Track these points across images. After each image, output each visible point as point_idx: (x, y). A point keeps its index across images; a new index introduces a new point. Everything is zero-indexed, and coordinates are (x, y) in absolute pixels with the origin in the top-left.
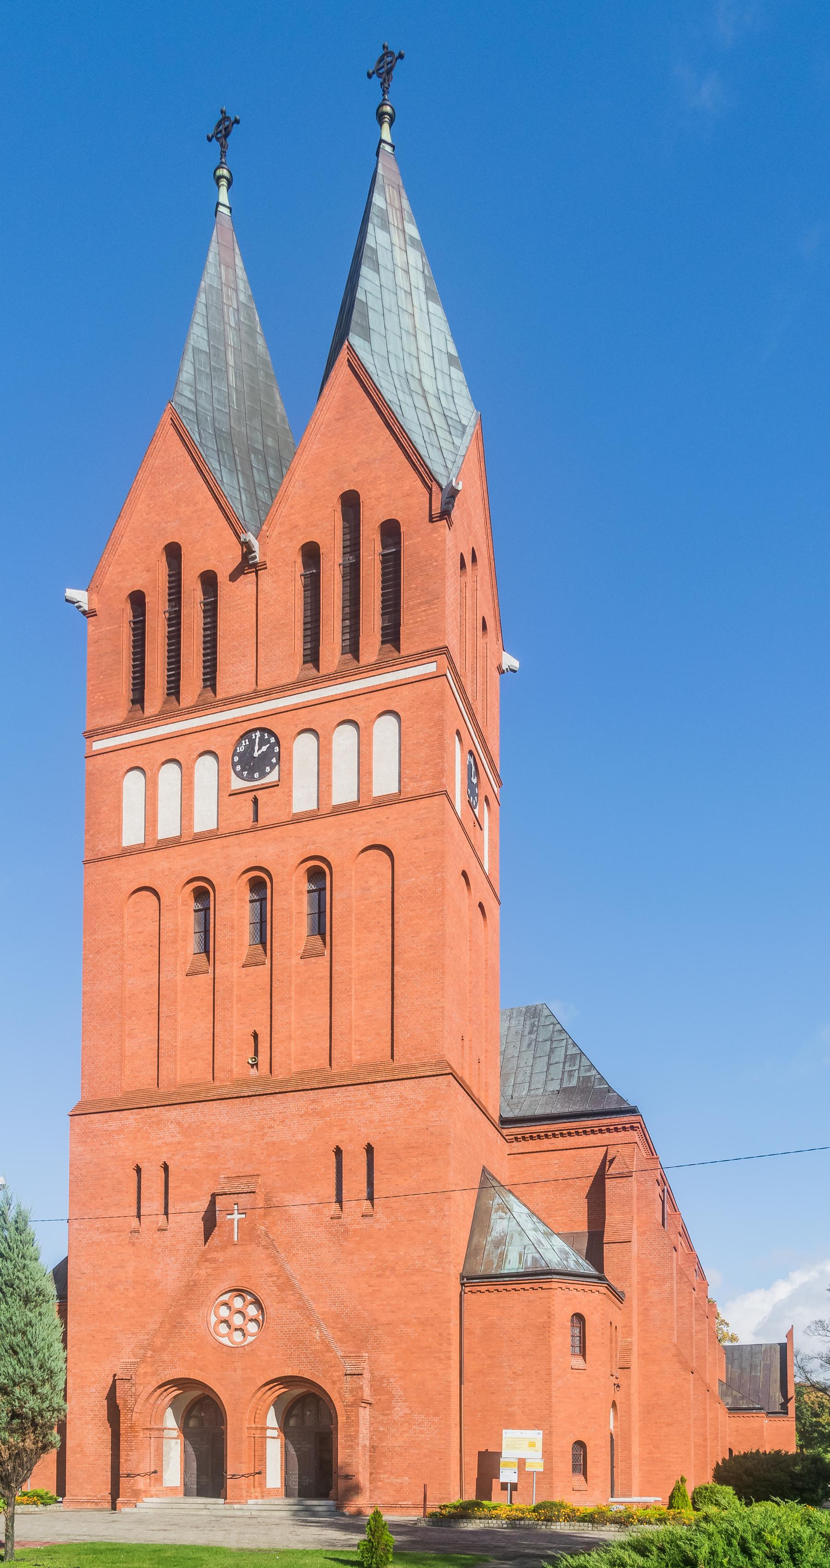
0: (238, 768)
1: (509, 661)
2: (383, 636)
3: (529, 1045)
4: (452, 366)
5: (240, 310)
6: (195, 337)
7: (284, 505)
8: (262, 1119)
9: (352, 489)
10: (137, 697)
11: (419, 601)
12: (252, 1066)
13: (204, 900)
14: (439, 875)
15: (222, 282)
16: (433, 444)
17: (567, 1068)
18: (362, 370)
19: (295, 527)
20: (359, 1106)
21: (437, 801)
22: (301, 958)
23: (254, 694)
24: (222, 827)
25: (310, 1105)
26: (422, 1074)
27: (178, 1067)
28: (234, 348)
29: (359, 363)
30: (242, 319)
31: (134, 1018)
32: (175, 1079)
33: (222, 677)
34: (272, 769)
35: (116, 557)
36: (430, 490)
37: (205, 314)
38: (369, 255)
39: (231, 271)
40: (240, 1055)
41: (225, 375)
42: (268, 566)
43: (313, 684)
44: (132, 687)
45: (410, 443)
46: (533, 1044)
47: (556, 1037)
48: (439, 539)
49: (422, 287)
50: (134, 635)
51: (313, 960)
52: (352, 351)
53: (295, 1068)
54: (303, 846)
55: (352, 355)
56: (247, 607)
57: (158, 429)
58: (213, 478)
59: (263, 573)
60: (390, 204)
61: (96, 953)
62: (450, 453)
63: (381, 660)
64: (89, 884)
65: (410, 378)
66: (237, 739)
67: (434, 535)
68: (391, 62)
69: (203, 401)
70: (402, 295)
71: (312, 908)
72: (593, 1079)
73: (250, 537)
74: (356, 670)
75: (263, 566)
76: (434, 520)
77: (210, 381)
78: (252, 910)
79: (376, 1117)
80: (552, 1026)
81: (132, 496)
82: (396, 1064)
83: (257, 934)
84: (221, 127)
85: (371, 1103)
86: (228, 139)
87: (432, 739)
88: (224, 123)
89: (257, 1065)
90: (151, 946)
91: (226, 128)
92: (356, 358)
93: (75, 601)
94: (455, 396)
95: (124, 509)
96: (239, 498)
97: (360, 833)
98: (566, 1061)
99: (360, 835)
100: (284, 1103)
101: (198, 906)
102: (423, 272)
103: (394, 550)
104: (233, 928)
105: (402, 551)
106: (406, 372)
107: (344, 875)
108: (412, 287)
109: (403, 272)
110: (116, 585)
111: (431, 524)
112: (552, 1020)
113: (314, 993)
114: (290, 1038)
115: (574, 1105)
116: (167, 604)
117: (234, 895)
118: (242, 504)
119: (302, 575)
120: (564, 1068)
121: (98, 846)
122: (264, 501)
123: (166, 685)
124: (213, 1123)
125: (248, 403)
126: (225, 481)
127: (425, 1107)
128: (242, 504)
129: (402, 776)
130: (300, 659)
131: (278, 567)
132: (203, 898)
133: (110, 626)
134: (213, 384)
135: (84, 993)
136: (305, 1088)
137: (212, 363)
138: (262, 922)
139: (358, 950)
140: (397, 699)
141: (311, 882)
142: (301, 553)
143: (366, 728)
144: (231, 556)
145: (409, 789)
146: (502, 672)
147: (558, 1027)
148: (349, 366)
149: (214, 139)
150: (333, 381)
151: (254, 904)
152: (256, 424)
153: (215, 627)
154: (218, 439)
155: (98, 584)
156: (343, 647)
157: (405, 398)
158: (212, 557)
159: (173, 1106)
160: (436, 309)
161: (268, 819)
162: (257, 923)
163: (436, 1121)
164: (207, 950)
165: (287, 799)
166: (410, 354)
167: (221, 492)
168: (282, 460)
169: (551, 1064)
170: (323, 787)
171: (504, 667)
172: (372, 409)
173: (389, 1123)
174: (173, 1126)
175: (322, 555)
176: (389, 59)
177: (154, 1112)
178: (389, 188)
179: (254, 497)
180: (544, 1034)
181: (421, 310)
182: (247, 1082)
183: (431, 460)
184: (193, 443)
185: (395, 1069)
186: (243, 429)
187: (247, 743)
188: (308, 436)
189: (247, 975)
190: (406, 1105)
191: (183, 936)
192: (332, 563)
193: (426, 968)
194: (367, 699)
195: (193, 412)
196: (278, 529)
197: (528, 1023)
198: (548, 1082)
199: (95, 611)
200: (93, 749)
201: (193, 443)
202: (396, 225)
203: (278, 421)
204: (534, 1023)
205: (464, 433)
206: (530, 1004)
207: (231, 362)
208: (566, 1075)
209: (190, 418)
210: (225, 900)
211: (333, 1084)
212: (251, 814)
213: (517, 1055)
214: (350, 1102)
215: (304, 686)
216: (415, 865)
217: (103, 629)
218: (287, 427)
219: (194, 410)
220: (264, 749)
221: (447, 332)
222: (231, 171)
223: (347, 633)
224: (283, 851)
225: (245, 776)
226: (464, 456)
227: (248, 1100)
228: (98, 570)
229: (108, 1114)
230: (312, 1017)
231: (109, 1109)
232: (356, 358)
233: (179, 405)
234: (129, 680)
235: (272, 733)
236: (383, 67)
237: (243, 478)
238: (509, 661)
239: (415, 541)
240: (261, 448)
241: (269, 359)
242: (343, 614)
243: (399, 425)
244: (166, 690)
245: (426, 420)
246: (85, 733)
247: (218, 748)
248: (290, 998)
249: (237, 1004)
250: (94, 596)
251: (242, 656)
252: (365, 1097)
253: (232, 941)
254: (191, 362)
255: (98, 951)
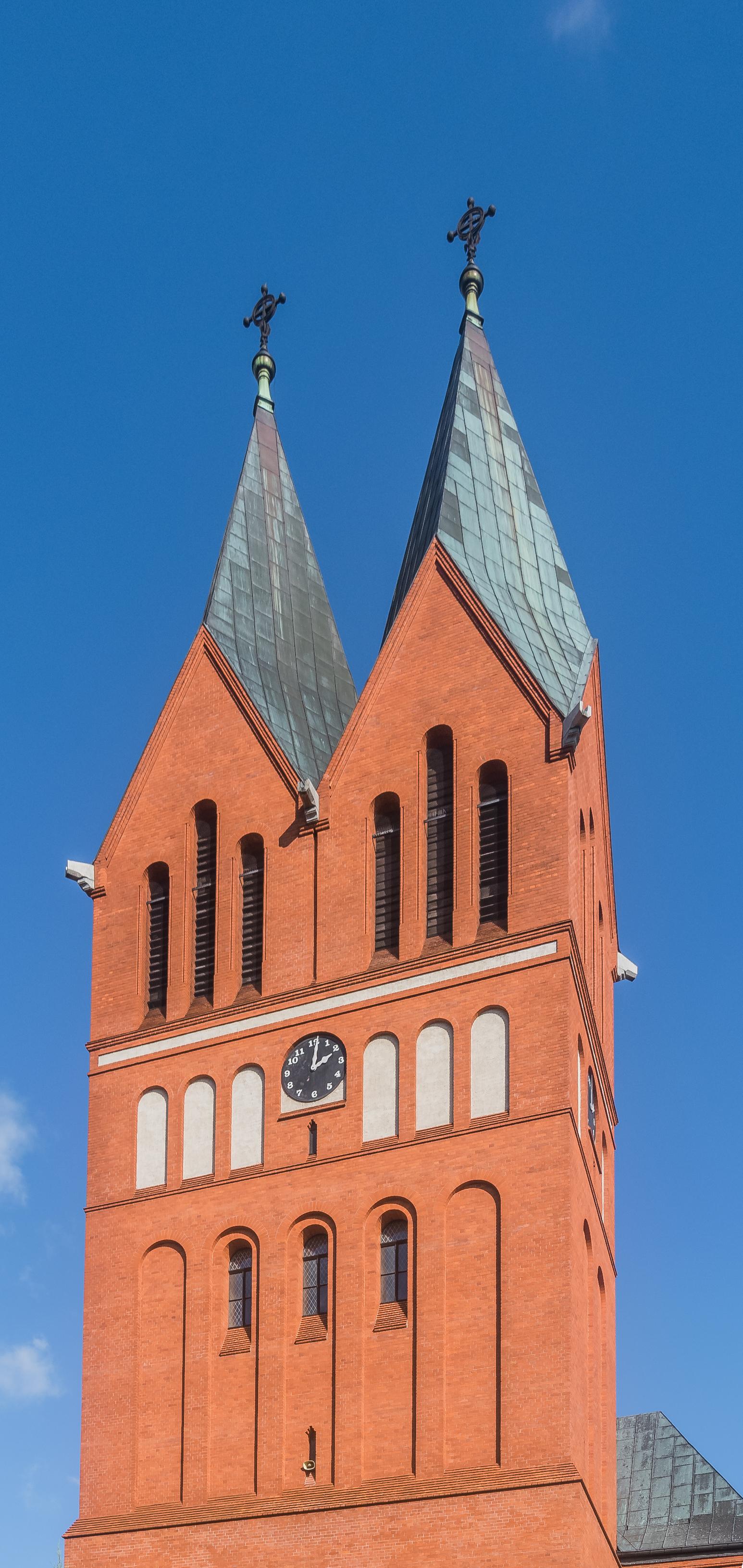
0: (290, 1085)
1: (626, 965)
2: (482, 912)
3: (644, 1463)
4: (561, 581)
5: (286, 523)
6: (232, 549)
7: (352, 747)
8: (322, 1542)
9: (442, 723)
10: (156, 997)
11: (532, 863)
12: (308, 1473)
13: (243, 1259)
14: (561, 1219)
15: (264, 489)
16: (547, 667)
17: (697, 1492)
18: (456, 574)
19: (367, 774)
20: (455, 1526)
21: (559, 1122)
22: (374, 1331)
23: (312, 989)
24: (269, 1163)
25: (387, 1523)
26: (540, 1482)
27: (209, 1474)
28: (279, 567)
29: (452, 565)
30: (288, 534)
31: (150, 1412)
32: (205, 1491)
33: (269, 969)
34: (334, 1087)
35: (131, 822)
36: (547, 721)
37: (244, 524)
38: (458, 441)
39: (274, 478)
40: (290, 1459)
41: (270, 598)
42: (331, 826)
43: (391, 974)
44: (149, 986)
45: (520, 663)
46: (649, 1461)
47: (679, 1452)
48: (558, 783)
49: (522, 485)
50: (152, 921)
51: (390, 1333)
52: (442, 550)
53: (365, 1476)
54: (378, 1184)
55: (442, 555)
56: (303, 878)
57: (188, 659)
58: (259, 717)
59: (324, 835)
60: (480, 386)
61: (101, 1327)
62: (567, 680)
63: (481, 940)
64: (92, 1238)
65: (512, 590)
66: (289, 1048)
67: (552, 779)
68: (478, 220)
69: (242, 627)
70: (498, 492)
71: (387, 1268)
72: (733, 1505)
73: (309, 785)
74: (449, 954)
75: (325, 825)
76: (551, 759)
77: (251, 603)
78: (307, 1270)
79: (478, 1540)
80: (672, 1439)
81: (154, 744)
82: (503, 1469)
83: (313, 1301)
84: (262, 307)
85: (470, 1521)
86: (269, 323)
87: (551, 1041)
88: (265, 303)
89: (313, 1472)
90: (174, 1317)
91: (268, 310)
92: (448, 559)
93: (78, 876)
94: (566, 617)
95: (143, 760)
96: (291, 743)
97: (454, 1166)
98: (695, 1483)
99: (454, 1169)
100: (352, 1521)
101: (235, 1267)
102: (523, 468)
103: (498, 800)
104: (282, 1292)
105: (509, 800)
106: (507, 583)
107: (432, 1221)
108: (510, 484)
109: (499, 466)
110: (130, 856)
111: (548, 765)
112: (672, 1431)
113: (391, 1377)
114: (359, 1436)
115: (714, 1536)
116: (196, 880)
117: (284, 1249)
118: (295, 750)
119: (375, 837)
120: (693, 1491)
121: (104, 1189)
122: (321, 749)
123: (194, 984)
124: (256, 1548)
125: (297, 634)
126: (273, 721)
127: (545, 1526)
128: (295, 750)
129: (511, 1090)
130: (372, 945)
131: (344, 826)
132: (241, 1256)
133: (122, 908)
134: (255, 608)
135: (85, 1379)
136: (381, 1500)
137: (253, 583)
138: (321, 1287)
139: (451, 1320)
140: (502, 991)
141: (386, 1233)
142: (373, 808)
143: (461, 1029)
144: (281, 815)
145: (520, 1107)
146: (617, 979)
147: (680, 1440)
148: (437, 569)
149: (252, 323)
150: (416, 589)
151: (310, 1262)
152: (308, 659)
153: (260, 908)
154: (262, 672)
155: (107, 855)
156: (428, 928)
157: (508, 611)
158: (257, 817)
159: (203, 1526)
160: (540, 513)
161: (330, 1150)
162: (314, 1287)
163: (560, 1544)
164: (247, 1323)
165: (356, 1123)
166: (511, 563)
167: (269, 733)
168: (339, 705)
169: (675, 1487)
170: (404, 1108)
171: (620, 973)
172: (469, 622)
173: (496, 1547)
174: (202, 1551)
175: (402, 809)
176: (476, 217)
177: (176, 1534)
178: (478, 367)
179: (309, 743)
180: (661, 1450)
181: (522, 512)
182: (300, 1494)
183: (546, 684)
184: (232, 674)
185: (503, 1475)
186: (293, 664)
187: (302, 1053)
188: (384, 659)
189: (301, 1355)
190: (519, 1523)
191: (216, 1305)
192: (415, 819)
193: (544, 1342)
194: (463, 992)
195: (230, 639)
196: (344, 778)
197: (641, 1435)
198: (674, 1509)
199: (104, 890)
200: (99, 1065)
201: (232, 674)
202: (488, 410)
203: (334, 657)
204: (648, 1435)
205: (580, 660)
206: (644, 1412)
207: (277, 584)
208: (696, 1500)
209: (227, 645)
210: (273, 1256)
211: (419, 1496)
212: (307, 1144)
213: (628, 1475)
214: (442, 1519)
215: (378, 978)
216: (529, 1207)
217: (113, 913)
218: (345, 667)
219: (233, 637)
220: (325, 1059)
221: (553, 542)
222: (274, 359)
223: (433, 910)
224: (350, 1192)
225: (299, 1095)
226: (585, 685)
227: (303, 1517)
228: (108, 837)
229: (115, 1535)
230: (388, 1408)
231: (117, 1530)
232: (448, 559)
233: (214, 629)
234: (146, 978)
235: (334, 1039)
236: (468, 227)
237: (295, 720)
238: (626, 965)
239: (526, 787)
240: (314, 689)
241: (322, 584)
242: (428, 886)
243: (504, 640)
244: (193, 989)
245: (535, 639)
246: (89, 1044)
247: (263, 1060)
248: (360, 1383)
249: (287, 1392)
250: (103, 871)
251: (296, 941)
252: (462, 1513)
253: (282, 1309)
254: (229, 580)
255: (104, 1324)
